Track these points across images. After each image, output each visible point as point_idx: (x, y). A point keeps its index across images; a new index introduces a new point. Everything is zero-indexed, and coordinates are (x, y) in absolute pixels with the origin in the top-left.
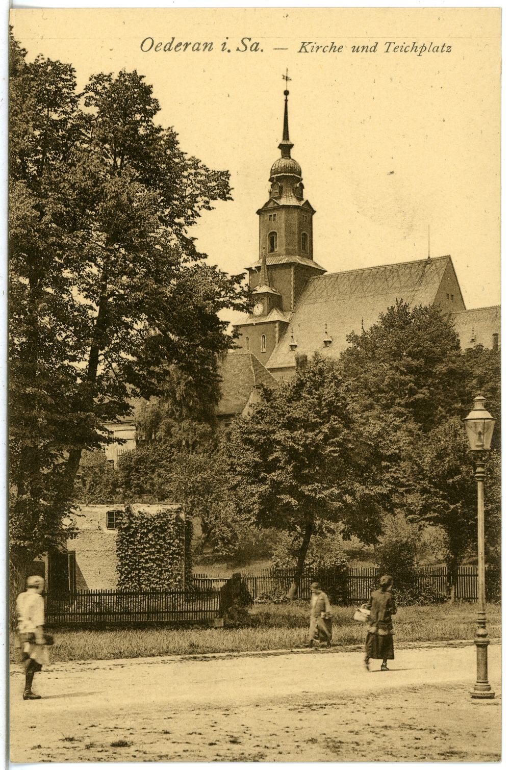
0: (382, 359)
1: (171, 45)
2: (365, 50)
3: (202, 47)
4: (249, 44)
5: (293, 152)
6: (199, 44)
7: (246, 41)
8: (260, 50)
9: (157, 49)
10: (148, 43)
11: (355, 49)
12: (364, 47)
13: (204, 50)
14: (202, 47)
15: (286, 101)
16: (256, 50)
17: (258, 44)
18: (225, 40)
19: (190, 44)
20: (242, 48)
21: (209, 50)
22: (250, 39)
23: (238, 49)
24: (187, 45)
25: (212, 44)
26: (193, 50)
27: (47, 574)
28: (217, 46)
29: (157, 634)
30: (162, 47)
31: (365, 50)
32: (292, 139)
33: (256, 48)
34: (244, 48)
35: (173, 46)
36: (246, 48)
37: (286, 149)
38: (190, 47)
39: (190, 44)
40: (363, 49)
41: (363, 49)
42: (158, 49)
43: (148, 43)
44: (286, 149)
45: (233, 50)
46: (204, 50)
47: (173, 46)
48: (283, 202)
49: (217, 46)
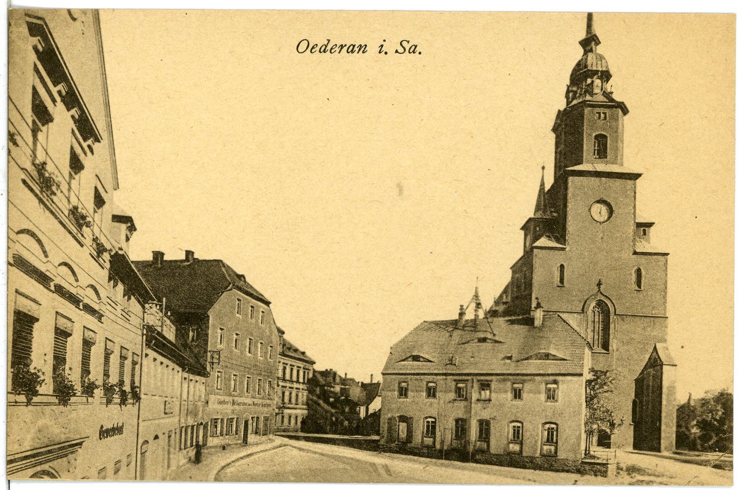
0: (705, 235)
1: (326, 46)
2: (363, 49)
3: (356, 49)
4: (407, 46)
6: (354, 46)
7: (404, 44)
8: (417, 53)
9: (313, 51)
10: (303, 46)
11: (363, 48)
12: (361, 45)
13: (358, 53)
14: (356, 49)
16: (414, 52)
17: (416, 46)
18: (383, 43)
19: (346, 45)
20: (401, 50)
21: (363, 52)
22: (408, 42)
23: (397, 51)
24: (342, 47)
25: (366, 46)
26: (320, 52)
27: (342, 437)
28: (373, 49)
29: (361, 453)
30: (318, 49)
31: (363, 49)
33: (413, 50)
34: (403, 51)
35: (329, 48)
36: (405, 50)
38: (345, 49)
39: (346, 45)
40: (360, 50)
41: (360, 50)
42: (313, 51)
43: (303, 46)
45: (391, 52)
46: (358, 53)
47: (329, 48)
49: (373, 49)
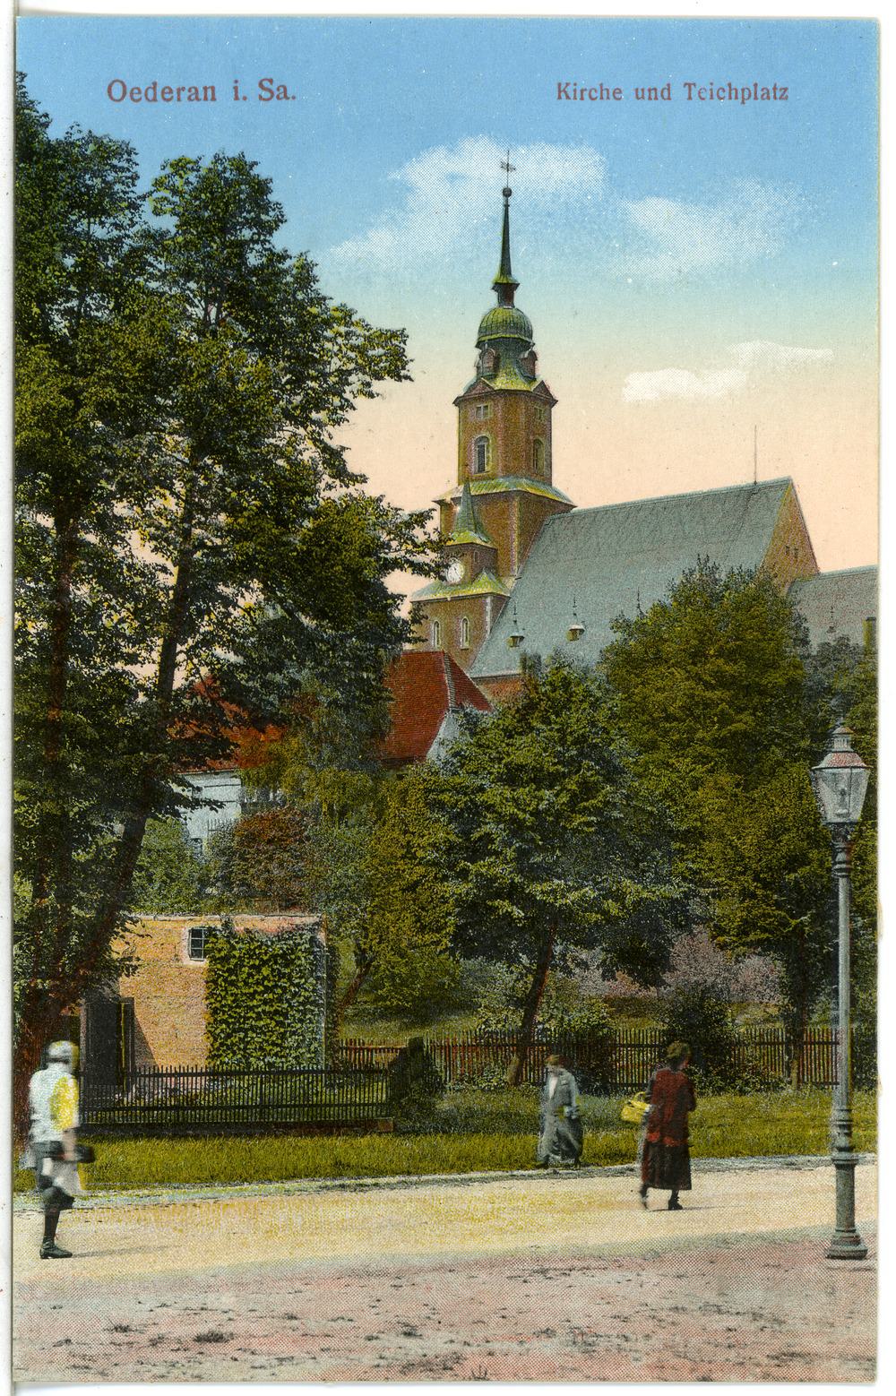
5: (518, 294)
15: (507, 206)
28: (224, 92)
32: (517, 273)
37: (506, 290)
44: (506, 290)
48: (500, 383)
49: (224, 92)
